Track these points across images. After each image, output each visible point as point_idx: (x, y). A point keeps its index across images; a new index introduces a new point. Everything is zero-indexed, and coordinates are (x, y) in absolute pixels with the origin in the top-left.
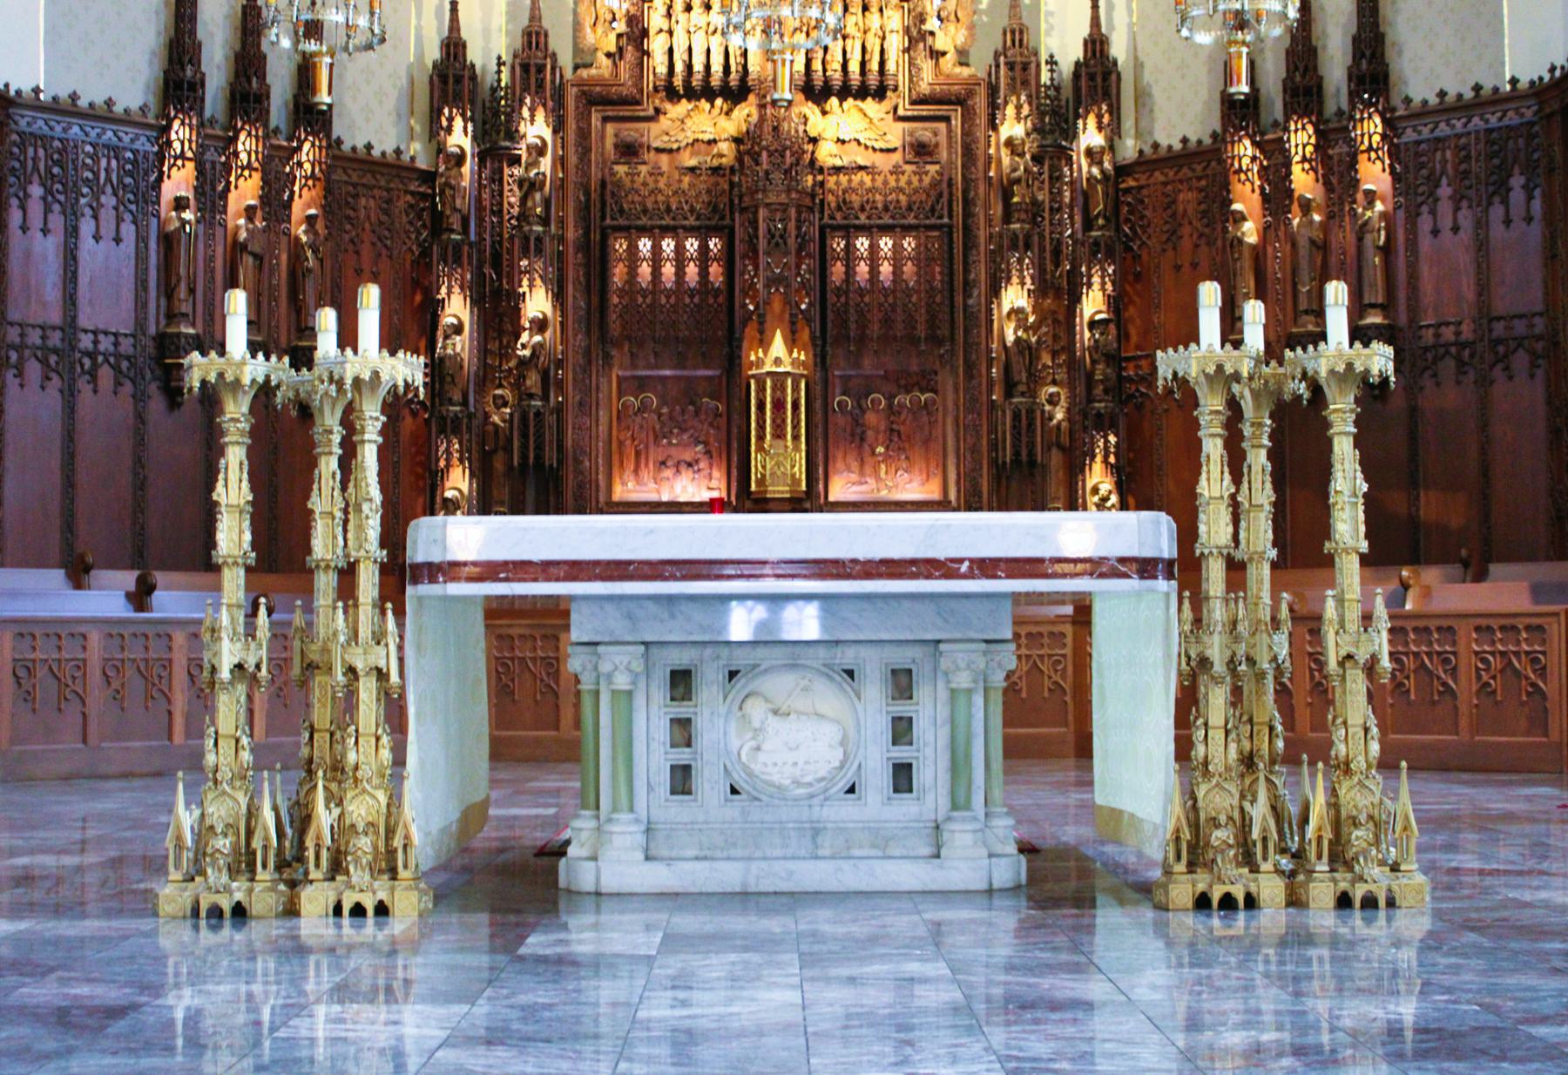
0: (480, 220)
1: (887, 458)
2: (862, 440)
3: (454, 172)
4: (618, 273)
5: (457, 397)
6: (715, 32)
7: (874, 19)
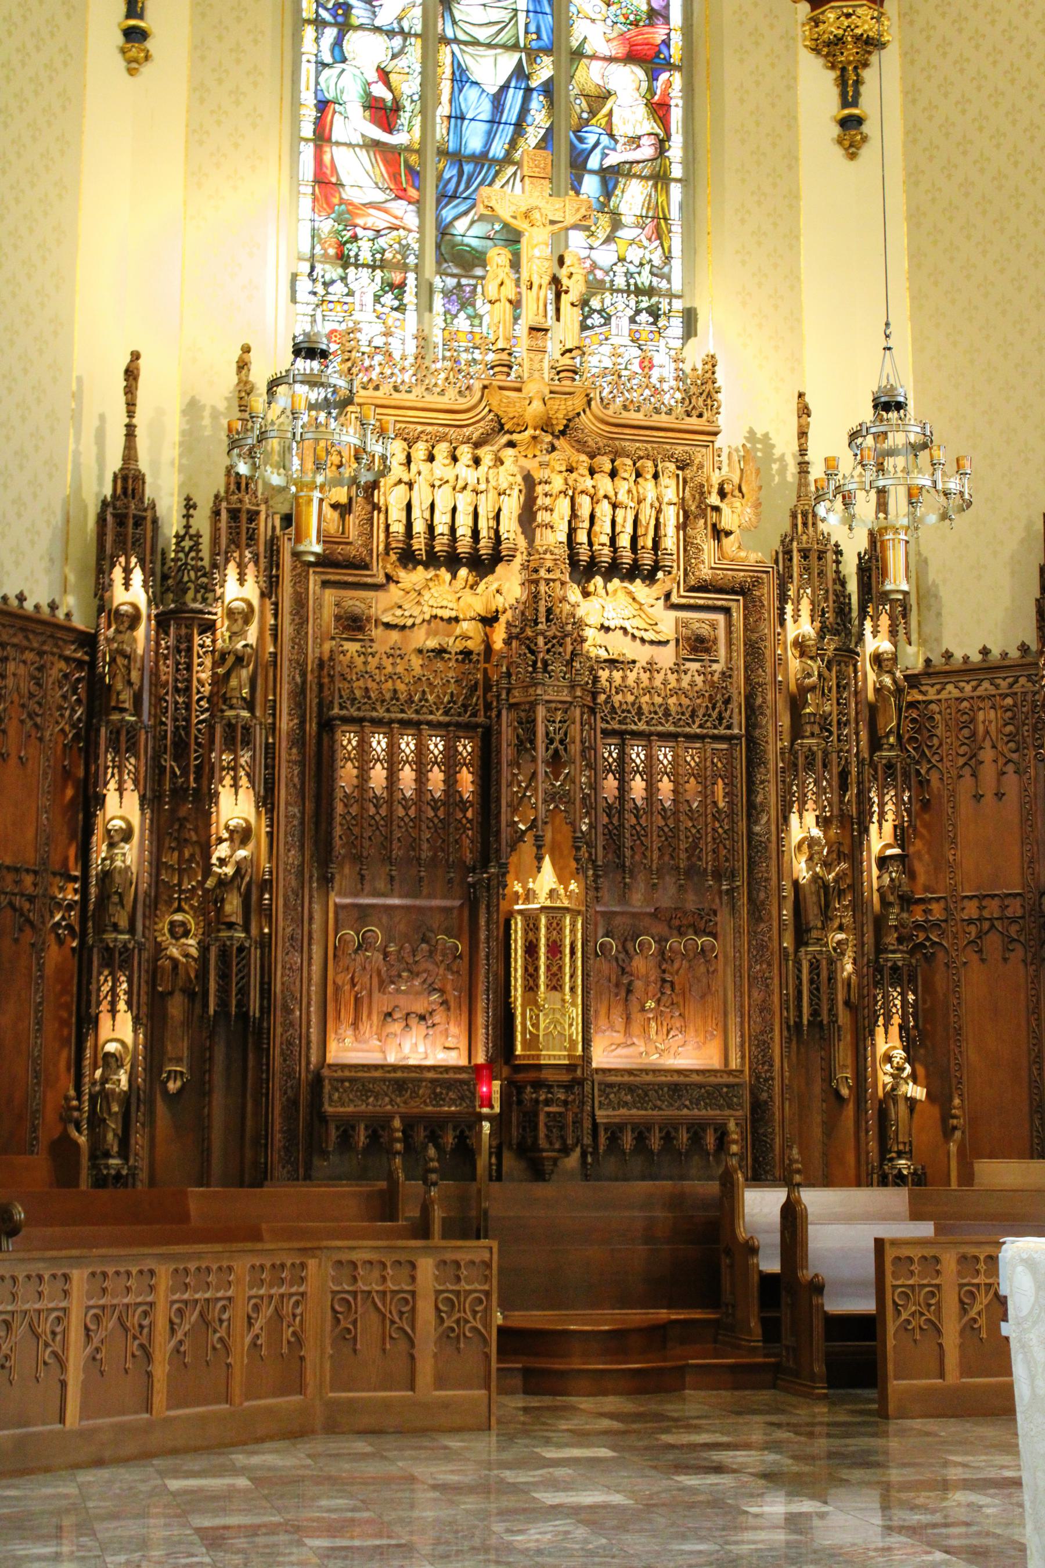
0: (158, 700)
1: (659, 1015)
2: (629, 991)
3: (126, 637)
4: (347, 774)
5: (123, 923)
6: (464, 488)
7: (648, 488)
